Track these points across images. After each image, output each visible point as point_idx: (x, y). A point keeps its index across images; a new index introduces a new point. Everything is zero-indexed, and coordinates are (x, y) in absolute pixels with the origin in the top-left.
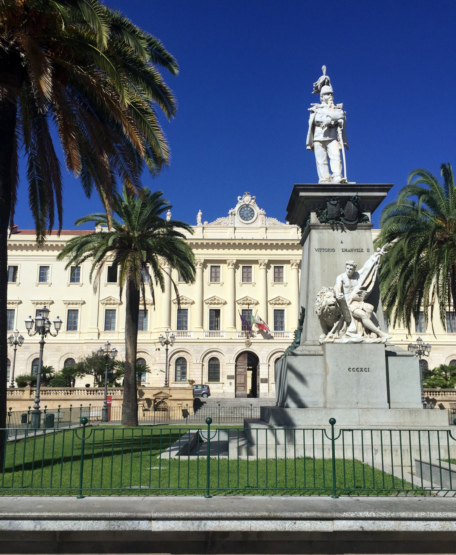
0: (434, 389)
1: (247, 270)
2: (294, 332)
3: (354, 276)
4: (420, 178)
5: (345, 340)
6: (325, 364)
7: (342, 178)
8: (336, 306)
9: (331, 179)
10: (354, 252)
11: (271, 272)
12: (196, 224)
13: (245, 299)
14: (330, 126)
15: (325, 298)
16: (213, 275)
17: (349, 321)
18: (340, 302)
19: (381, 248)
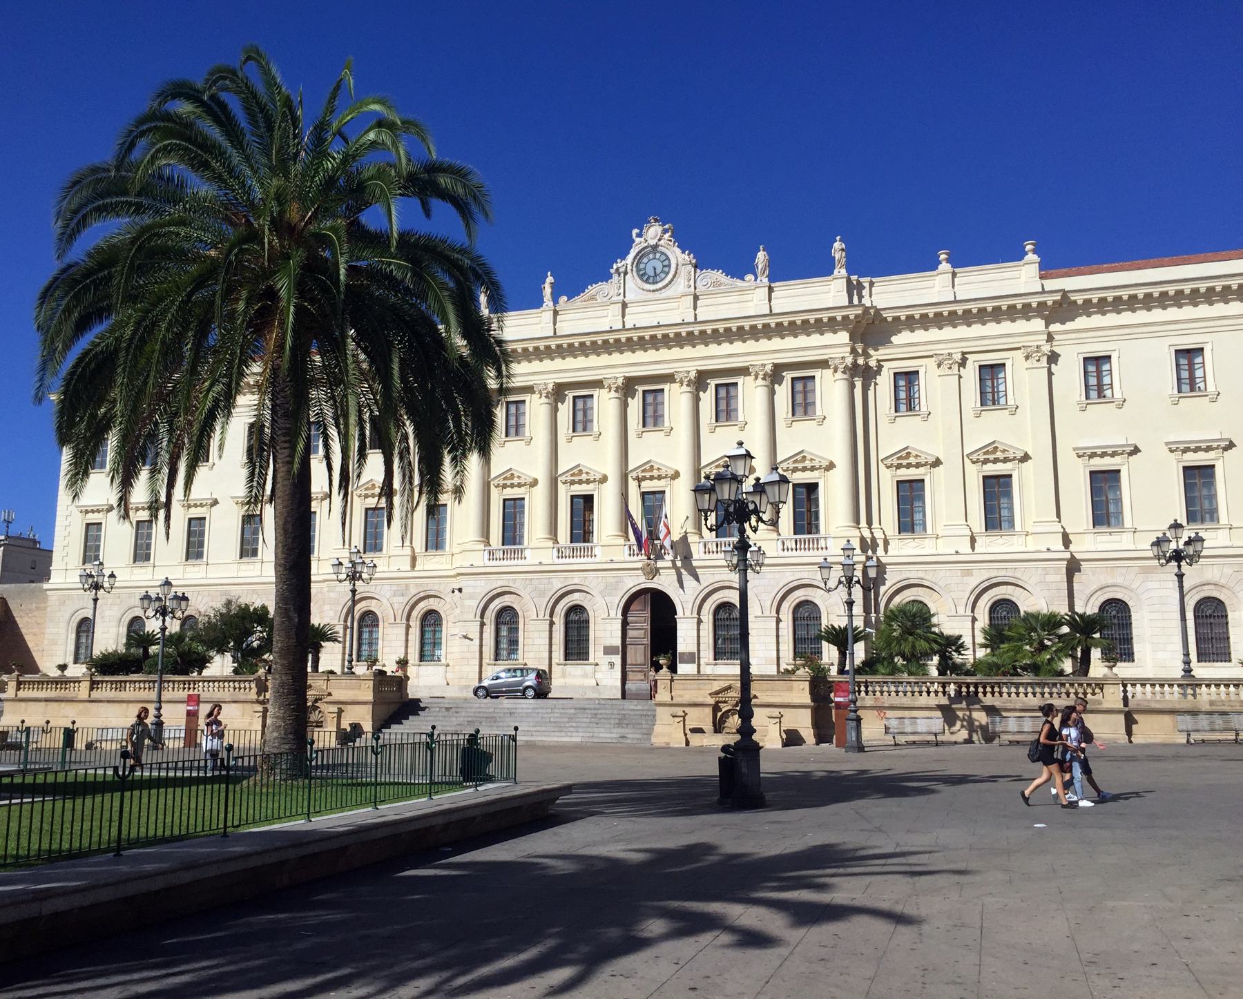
0: (1016, 680)
13: (647, 467)
16: (799, 399)
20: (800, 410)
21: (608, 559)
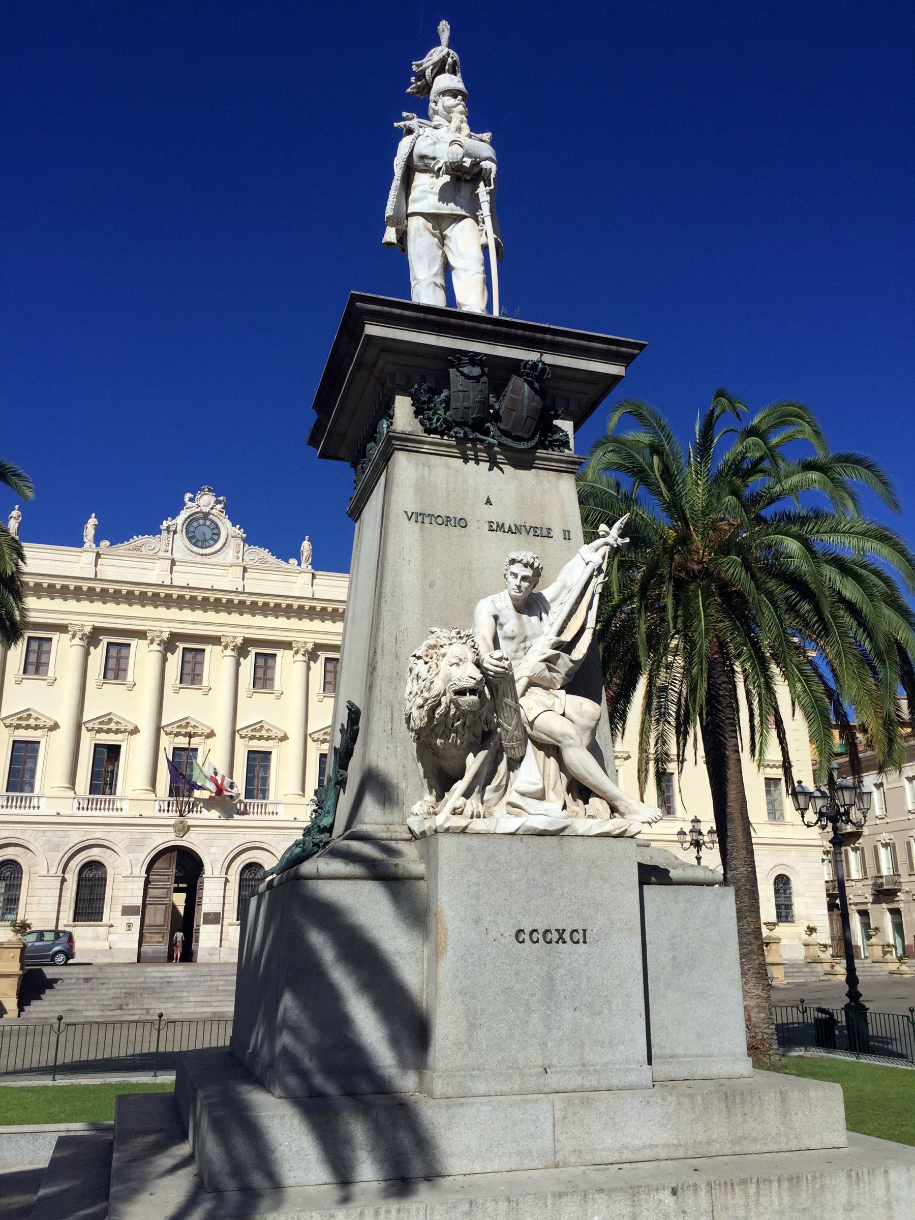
3: (531, 604)
8: (481, 695)
10: (522, 537)
16: (112, 663)
19: (610, 527)
20: (32, 668)
21: (137, 814)
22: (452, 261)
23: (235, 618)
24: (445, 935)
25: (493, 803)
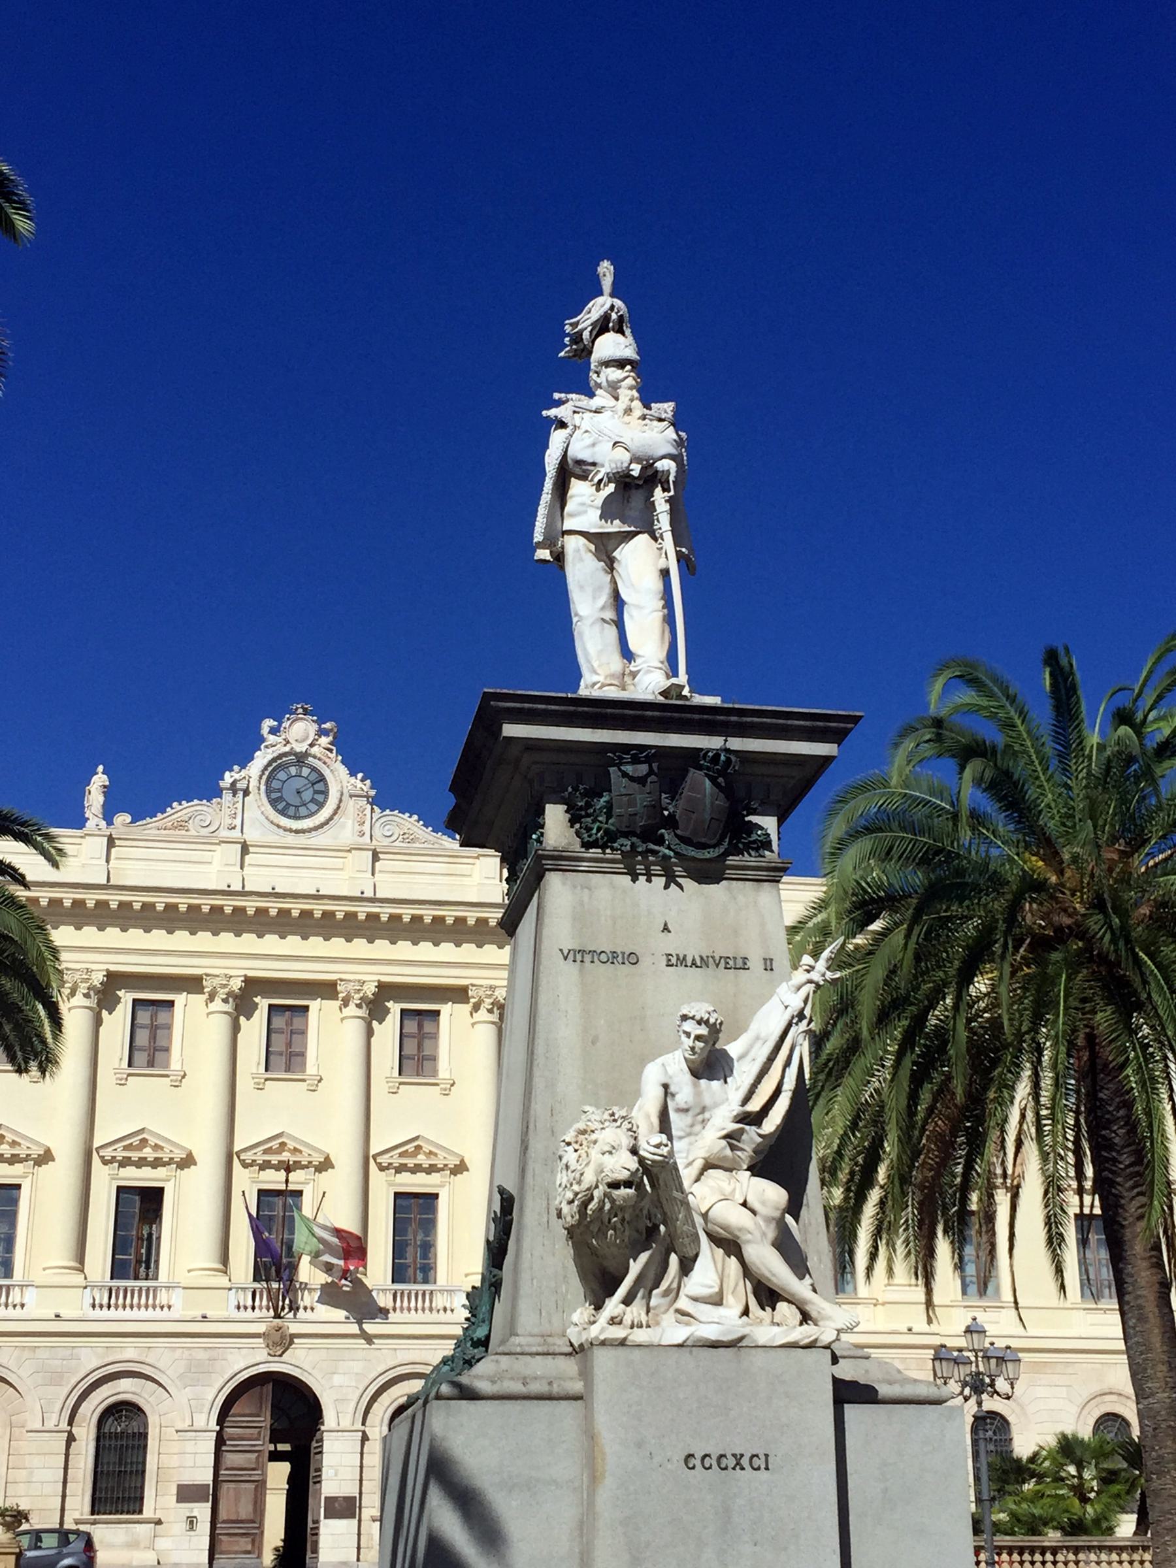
1: (289, 1023)
2: (468, 1295)
3: (711, 1064)
4: (967, 696)
5: (674, 1332)
6: (590, 1435)
7: (668, 677)
8: (640, 1187)
9: (627, 679)
11: (388, 1032)
12: (78, 821)
14: (623, 480)
15: (594, 1153)
16: (143, 1037)
17: (691, 1254)
18: (655, 1170)
21: (198, 1314)
22: (624, 595)
23: (360, 948)
24: (603, 1460)
25: (663, 1310)
